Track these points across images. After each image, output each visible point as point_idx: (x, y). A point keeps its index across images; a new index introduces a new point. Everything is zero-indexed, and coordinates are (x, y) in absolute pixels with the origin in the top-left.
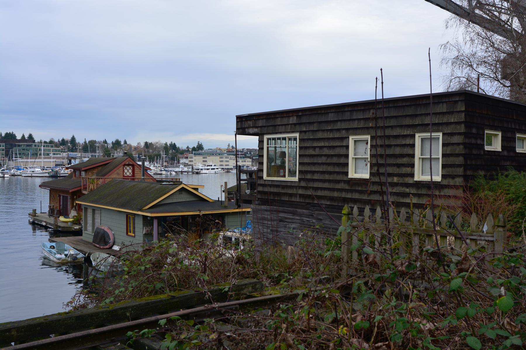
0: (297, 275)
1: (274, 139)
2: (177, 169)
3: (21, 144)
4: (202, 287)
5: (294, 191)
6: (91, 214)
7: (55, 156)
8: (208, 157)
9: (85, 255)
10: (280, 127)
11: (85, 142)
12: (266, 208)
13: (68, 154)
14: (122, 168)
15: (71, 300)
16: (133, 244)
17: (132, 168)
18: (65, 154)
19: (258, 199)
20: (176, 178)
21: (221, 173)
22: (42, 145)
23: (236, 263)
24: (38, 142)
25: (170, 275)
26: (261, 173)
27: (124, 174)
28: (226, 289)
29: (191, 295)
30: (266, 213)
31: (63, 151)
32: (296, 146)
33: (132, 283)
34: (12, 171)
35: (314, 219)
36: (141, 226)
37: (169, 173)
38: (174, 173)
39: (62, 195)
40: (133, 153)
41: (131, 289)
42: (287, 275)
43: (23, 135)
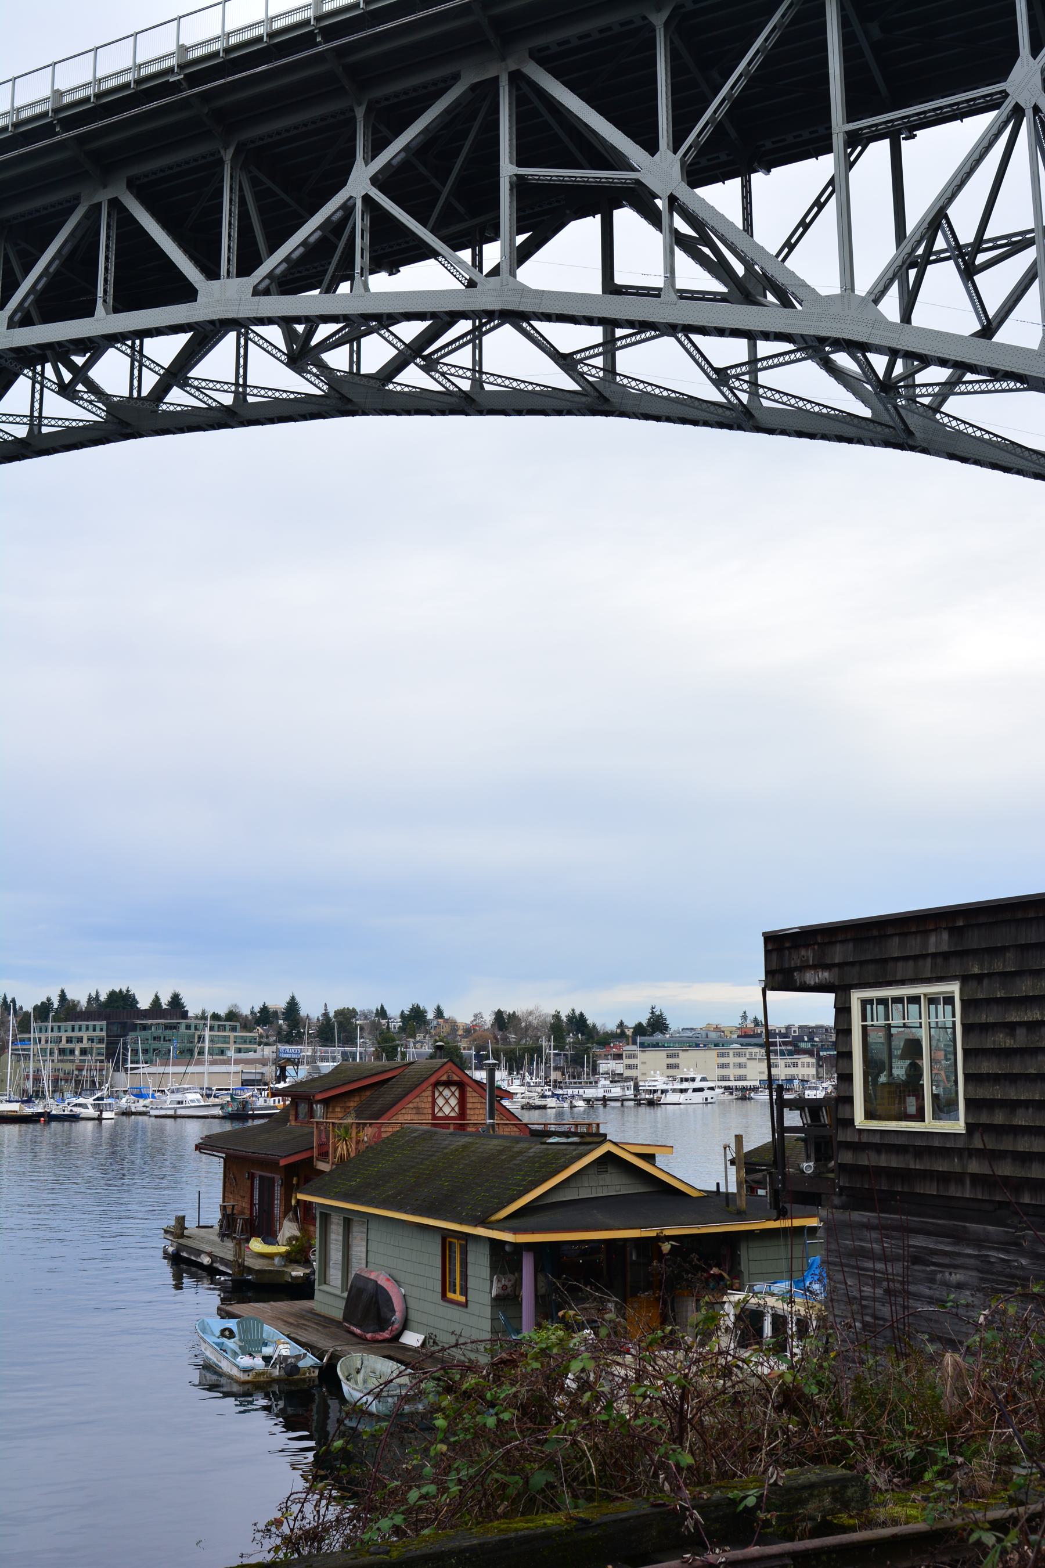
0: (977, 1453)
1: (882, 1001)
2: (590, 1093)
3: (150, 1021)
4: (672, 1490)
5: (954, 1165)
6: (341, 1230)
7: (242, 1056)
8: (681, 1054)
9: (321, 1360)
10: (900, 964)
11: (326, 1015)
12: (865, 1220)
13: (277, 1049)
14: (429, 1093)
15: (279, 1515)
16: (462, 1341)
17: (457, 1094)
18: (268, 1052)
19: (841, 1188)
20: (586, 1121)
21: (722, 1103)
22: (205, 1025)
23: (778, 1409)
24: (196, 1018)
25: (575, 1443)
26: (847, 1107)
27: (436, 1110)
28: (751, 1501)
29: (638, 1517)
30: (866, 1234)
31: (264, 1040)
32: (954, 1023)
33: (458, 1470)
34: (124, 1100)
35: (1024, 1257)
36: (486, 1272)
37: (566, 1105)
38: (581, 1104)
39: (258, 1173)
40: (463, 1044)
41: (455, 1489)
42: (944, 1453)
43: (157, 996)
